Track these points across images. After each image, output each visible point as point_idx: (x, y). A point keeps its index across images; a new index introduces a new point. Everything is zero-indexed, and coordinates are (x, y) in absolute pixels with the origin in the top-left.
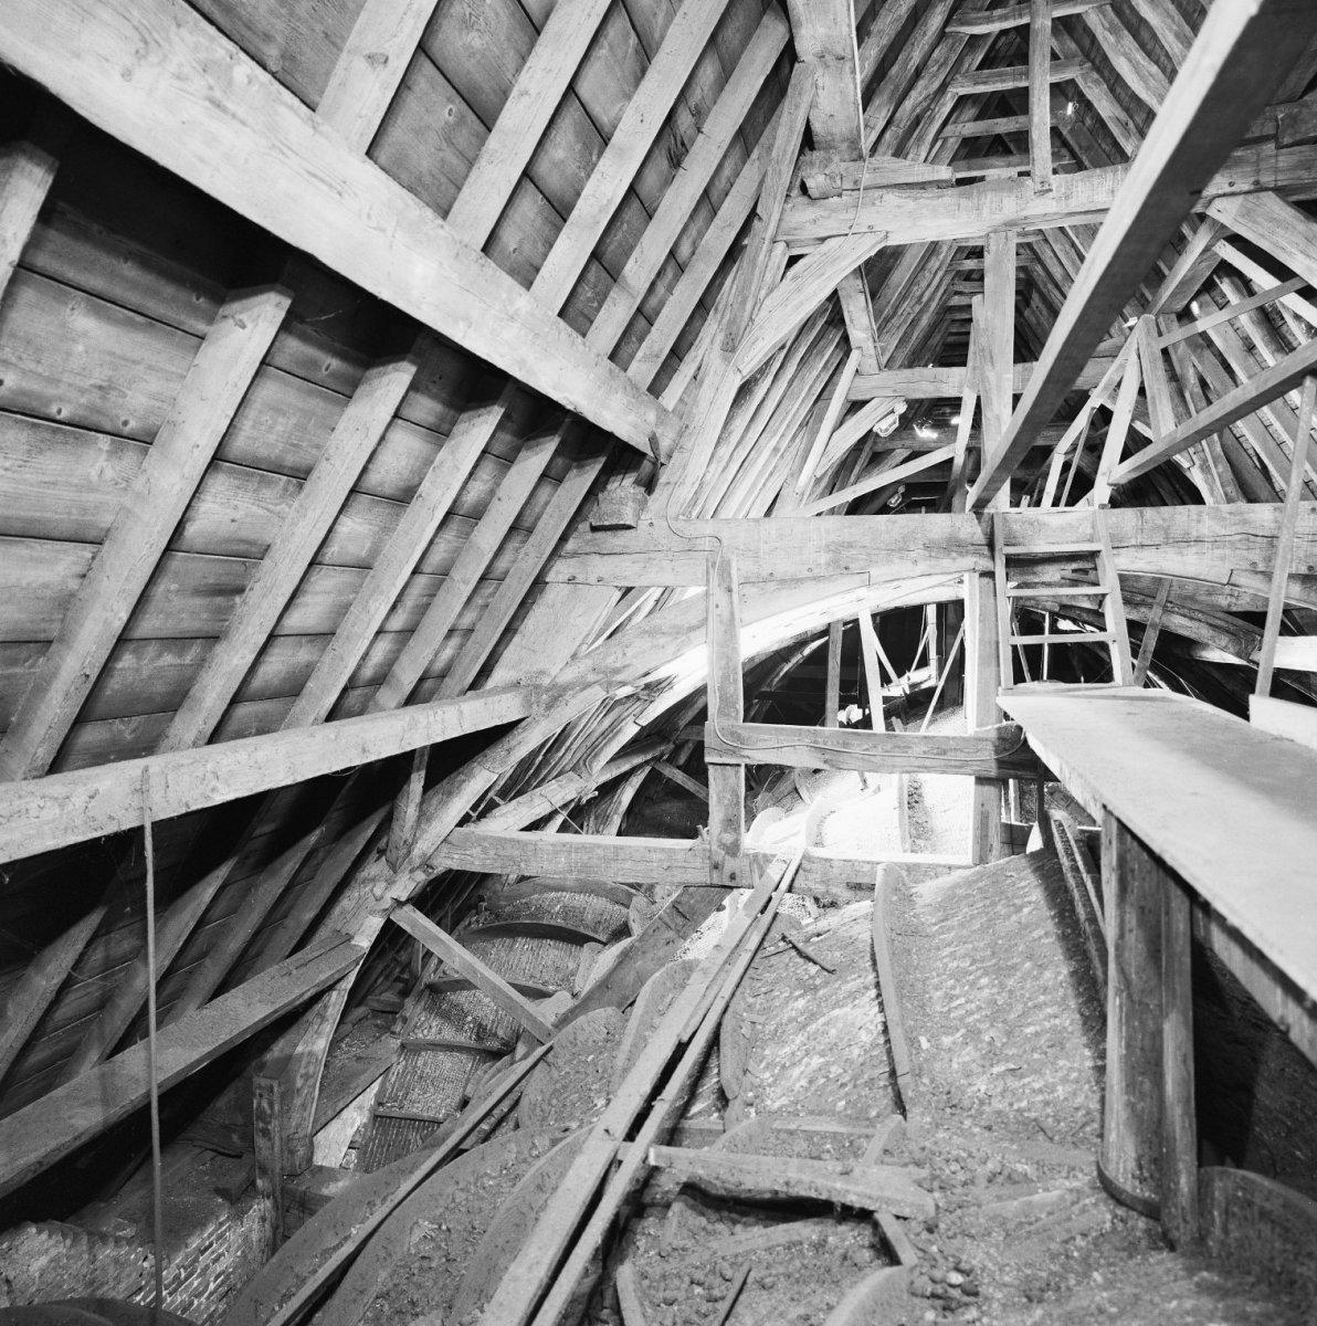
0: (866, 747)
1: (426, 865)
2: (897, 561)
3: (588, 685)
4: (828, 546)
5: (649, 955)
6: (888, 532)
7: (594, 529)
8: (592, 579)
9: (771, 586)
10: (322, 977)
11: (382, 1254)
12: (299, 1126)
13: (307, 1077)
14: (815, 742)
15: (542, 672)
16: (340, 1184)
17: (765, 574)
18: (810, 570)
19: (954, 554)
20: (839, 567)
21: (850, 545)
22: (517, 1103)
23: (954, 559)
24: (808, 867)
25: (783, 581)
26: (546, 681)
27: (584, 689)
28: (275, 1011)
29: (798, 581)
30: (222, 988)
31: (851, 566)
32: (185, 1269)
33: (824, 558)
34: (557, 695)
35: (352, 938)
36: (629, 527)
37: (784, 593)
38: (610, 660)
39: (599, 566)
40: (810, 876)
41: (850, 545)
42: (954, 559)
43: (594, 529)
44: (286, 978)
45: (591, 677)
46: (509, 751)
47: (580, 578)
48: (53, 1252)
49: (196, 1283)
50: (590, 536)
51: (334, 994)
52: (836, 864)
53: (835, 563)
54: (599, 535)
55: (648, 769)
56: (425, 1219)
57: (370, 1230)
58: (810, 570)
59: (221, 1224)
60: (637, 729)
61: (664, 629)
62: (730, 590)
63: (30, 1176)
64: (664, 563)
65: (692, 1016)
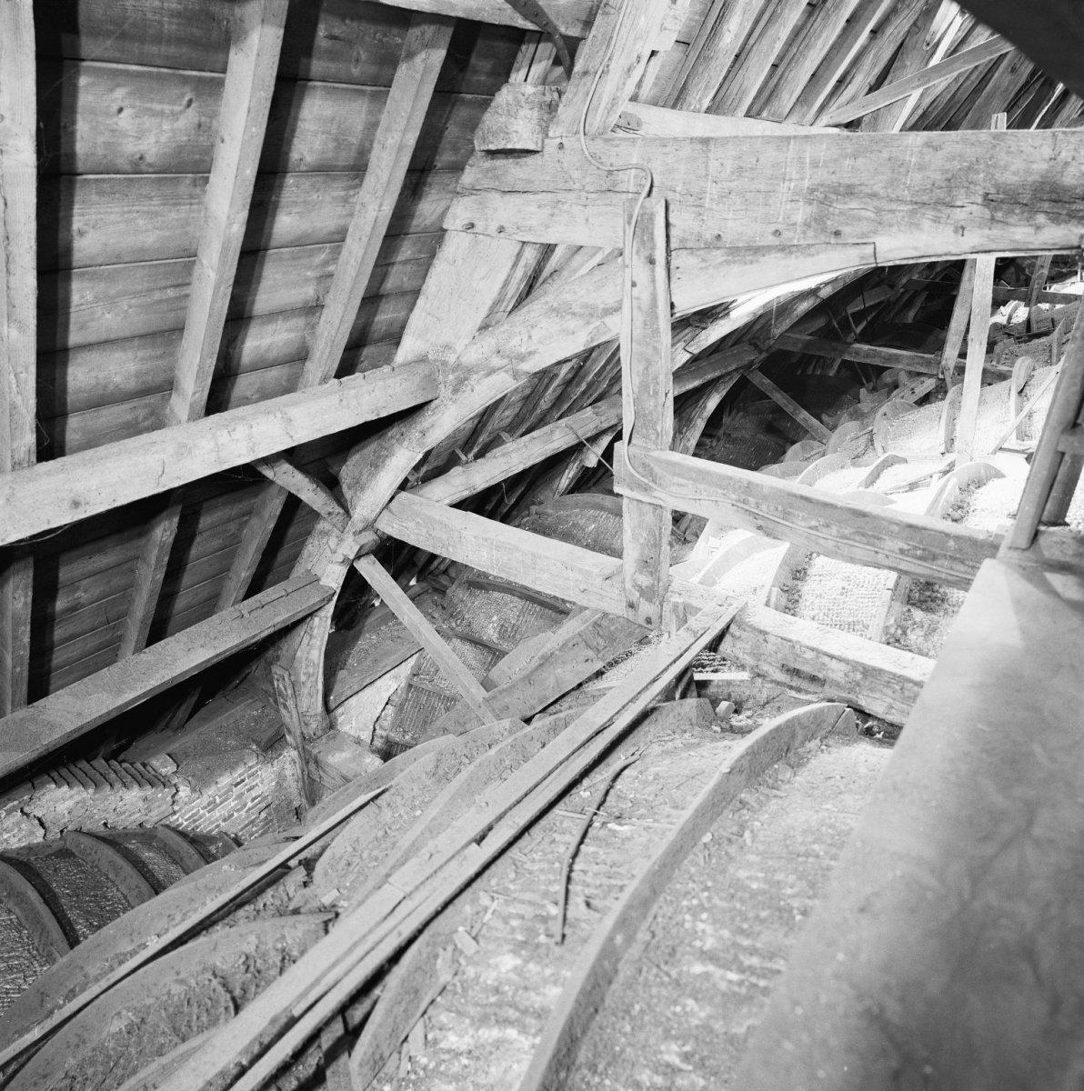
0: (814, 523)
1: (370, 526)
2: (926, 224)
3: (492, 371)
4: (812, 191)
5: (569, 667)
6: (921, 168)
7: (492, 154)
8: (493, 229)
9: (718, 256)
10: (278, 619)
11: (74, 1041)
12: (309, 708)
13: (309, 675)
14: (744, 502)
15: (447, 347)
16: (343, 755)
17: (708, 236)
18: (777, 233)
19: (1041, 218)
20: (824, 230)
21: (850, 191)
22: (324, 849)
23: (1038, 228)
24: (738, 634)
25: (734, 251)
26: (452, 359)
27: (488, 375)
28: (217, 656)
29: (757, 250)
30: (560, 418)
31: (846, 230)
32: (220, 797)
33: (802, 213)
34: (463, 376)
35: (318, 580)
36: (534, 152)
37: (735, 269)
38: (515, 341)
39: (503, 210)
40: (739, 644)
41: (850, 191)
42: (1038, 228)
43: (492, 154)
44: (238, 621)
45: (496, 361)
46: (423, 433)
47: (479, 227)
48: (77, 798)
49: (233, 804)
50: (488, 164)
51: (316, 620)
52: (771, 639)
53: (819, 221)
54: (500, 163)
55: (736, 378)
56: (128, 1009)
57: (85, 1002)
58: (777, 233)
59: (251, 768)
60: (688, 356)
61: (576, 309)
62: (652, 262)
63: (114, 715)
64: (576, 209)
65: (334, 965)
